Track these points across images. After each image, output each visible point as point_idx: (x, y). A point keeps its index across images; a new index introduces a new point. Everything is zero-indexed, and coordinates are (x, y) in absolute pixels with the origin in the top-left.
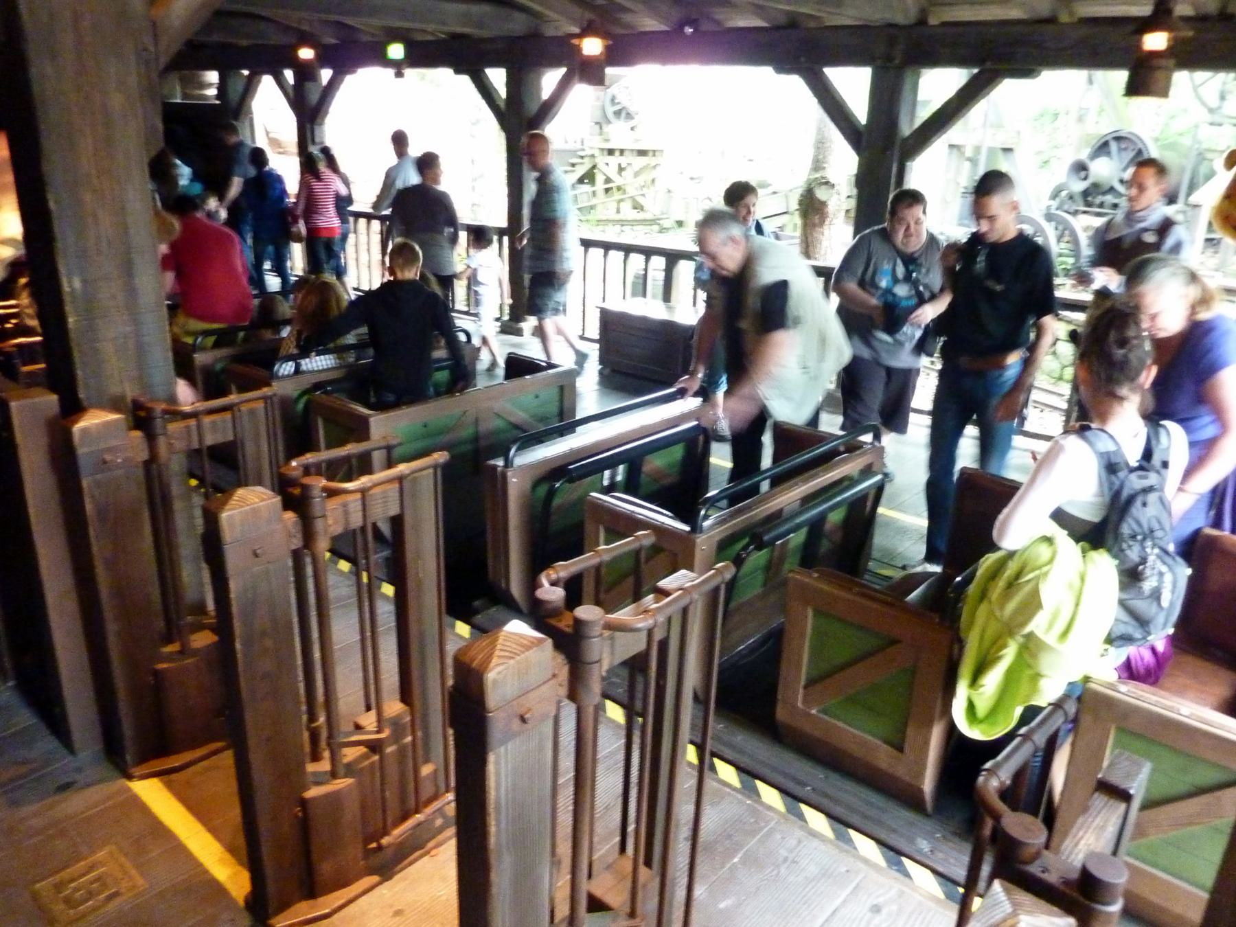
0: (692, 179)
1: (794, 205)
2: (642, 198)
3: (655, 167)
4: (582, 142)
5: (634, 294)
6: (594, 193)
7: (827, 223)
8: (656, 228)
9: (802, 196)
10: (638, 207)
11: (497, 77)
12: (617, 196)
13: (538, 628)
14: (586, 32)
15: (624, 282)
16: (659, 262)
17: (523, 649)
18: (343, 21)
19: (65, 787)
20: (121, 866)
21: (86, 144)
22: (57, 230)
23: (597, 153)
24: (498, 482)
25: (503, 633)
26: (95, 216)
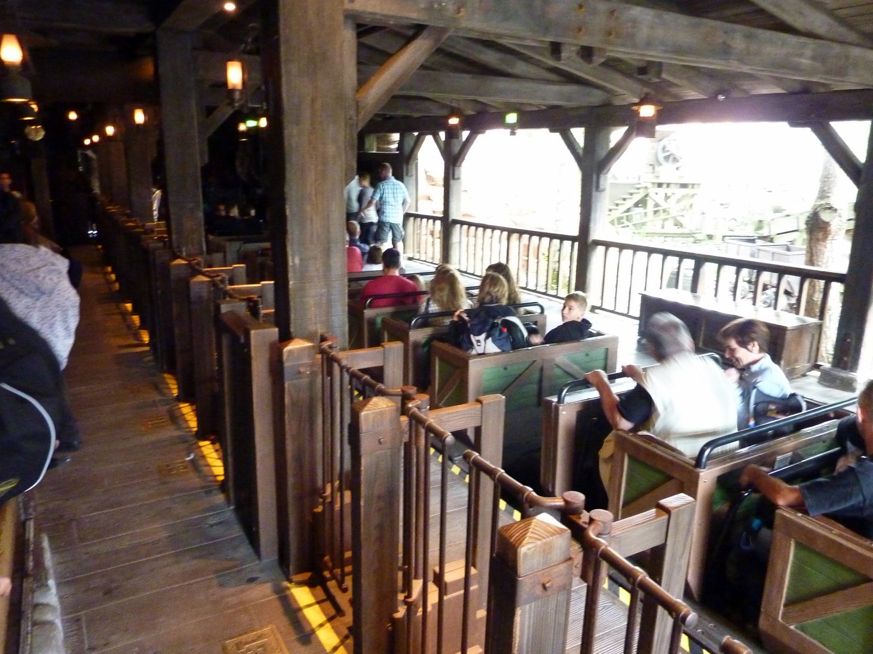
0: (722, 204)
1: (803, 226)
2: (681, 217)
3: (693, 196)
4: (639, 178)
5: (669, 286)
6: (645, 214)
7: (829, 238)
8: (692, 239)
9: (808, 217)
10: (678, 224)
11: (578, 134)
12: (663, 216)
13: (563, 521)
14: (643, 101)
15: (519, 247)
16: (689, 264)
17: (548, 535)
18: (478, 100)
19: (252, 580)
20: (277, 639)
21: (311, 176)
22: (289, 227)
23: (649, 185)
24: (552, 414)
25: (534, 520)
26: (312, 220)
